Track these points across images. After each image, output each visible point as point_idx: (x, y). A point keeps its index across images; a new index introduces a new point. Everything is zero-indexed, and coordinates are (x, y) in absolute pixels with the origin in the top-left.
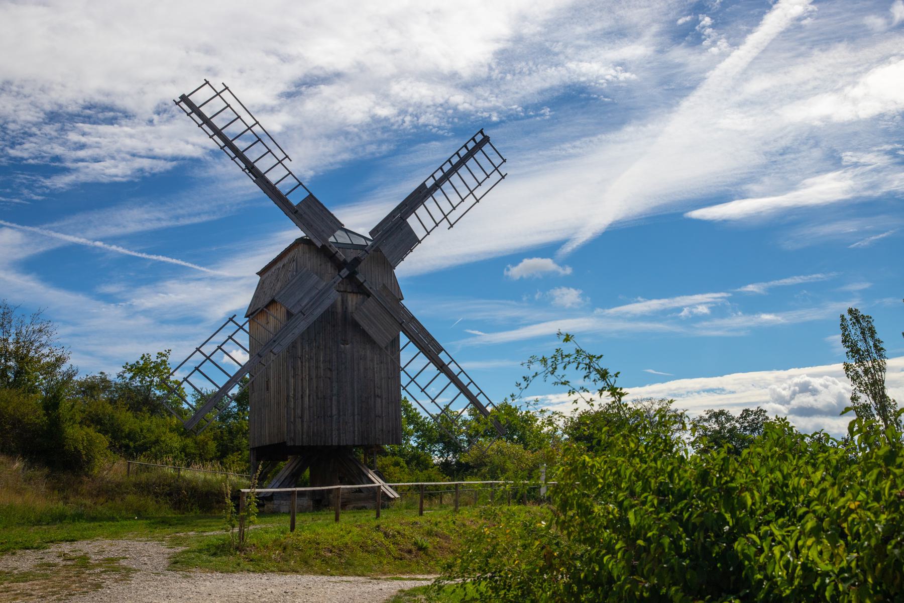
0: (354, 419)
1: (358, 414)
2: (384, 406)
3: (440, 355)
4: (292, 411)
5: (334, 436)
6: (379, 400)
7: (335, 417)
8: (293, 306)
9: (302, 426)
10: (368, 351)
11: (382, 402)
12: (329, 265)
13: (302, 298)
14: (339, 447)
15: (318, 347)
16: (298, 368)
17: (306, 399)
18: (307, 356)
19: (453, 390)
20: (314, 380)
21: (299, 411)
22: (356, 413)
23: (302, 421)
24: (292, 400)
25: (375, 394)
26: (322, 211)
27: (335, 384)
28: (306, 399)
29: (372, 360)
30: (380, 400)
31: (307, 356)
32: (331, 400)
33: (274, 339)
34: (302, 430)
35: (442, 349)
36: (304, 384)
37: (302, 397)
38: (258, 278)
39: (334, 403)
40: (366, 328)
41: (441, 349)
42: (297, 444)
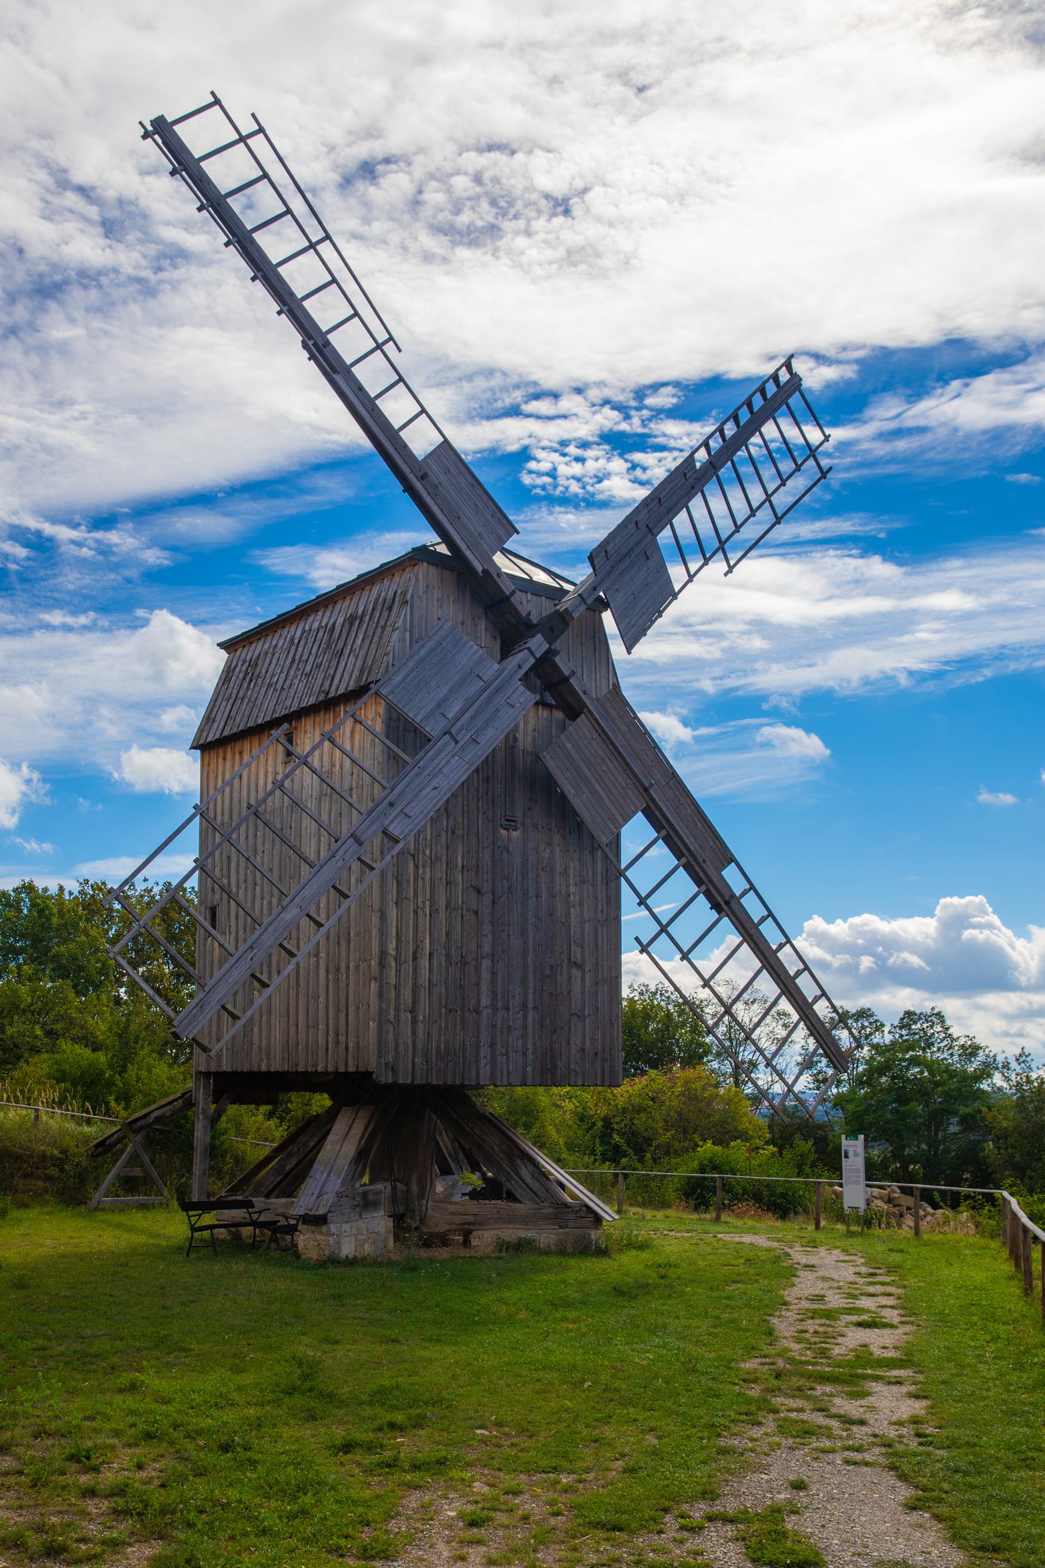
0: (525, 1018)
1: (535, 1008)
2: (587, 989)
3: (725, 873)
4: (393, 991)
5: (483, 1062)
6: (576, 973)
7: (486, 1013)
8: (427, 717)
9: (414, 1034)
10: (557, 851)
11: (583, 980)
12: (482, 624)
13: (444, 701)
14: (357, 1073)
15: (453, 832)
16: (408, 881)
17: (425, 962)
18: (428, 852)
19: (748, 960)
20: (442, 914)
21: (407, 995)
22: (530, 1005)
23: (414, 1021)
24: (393, 964)
25: (569, 959)
26: (473, 485)
27: (487, 929)
28: (425, 962)
29: (565, 873)
30: (579, 975)
31: (428, 852)
32: (478, 967)
33: (391, 798)
34: (414, 1042)
35: (731, 859)
36: (421, 922)
37: (415, 958)
38: (224, 655)
39: (485, 975)
40: (570, 793)
41: (728, 858)
42: (401, 1081)
